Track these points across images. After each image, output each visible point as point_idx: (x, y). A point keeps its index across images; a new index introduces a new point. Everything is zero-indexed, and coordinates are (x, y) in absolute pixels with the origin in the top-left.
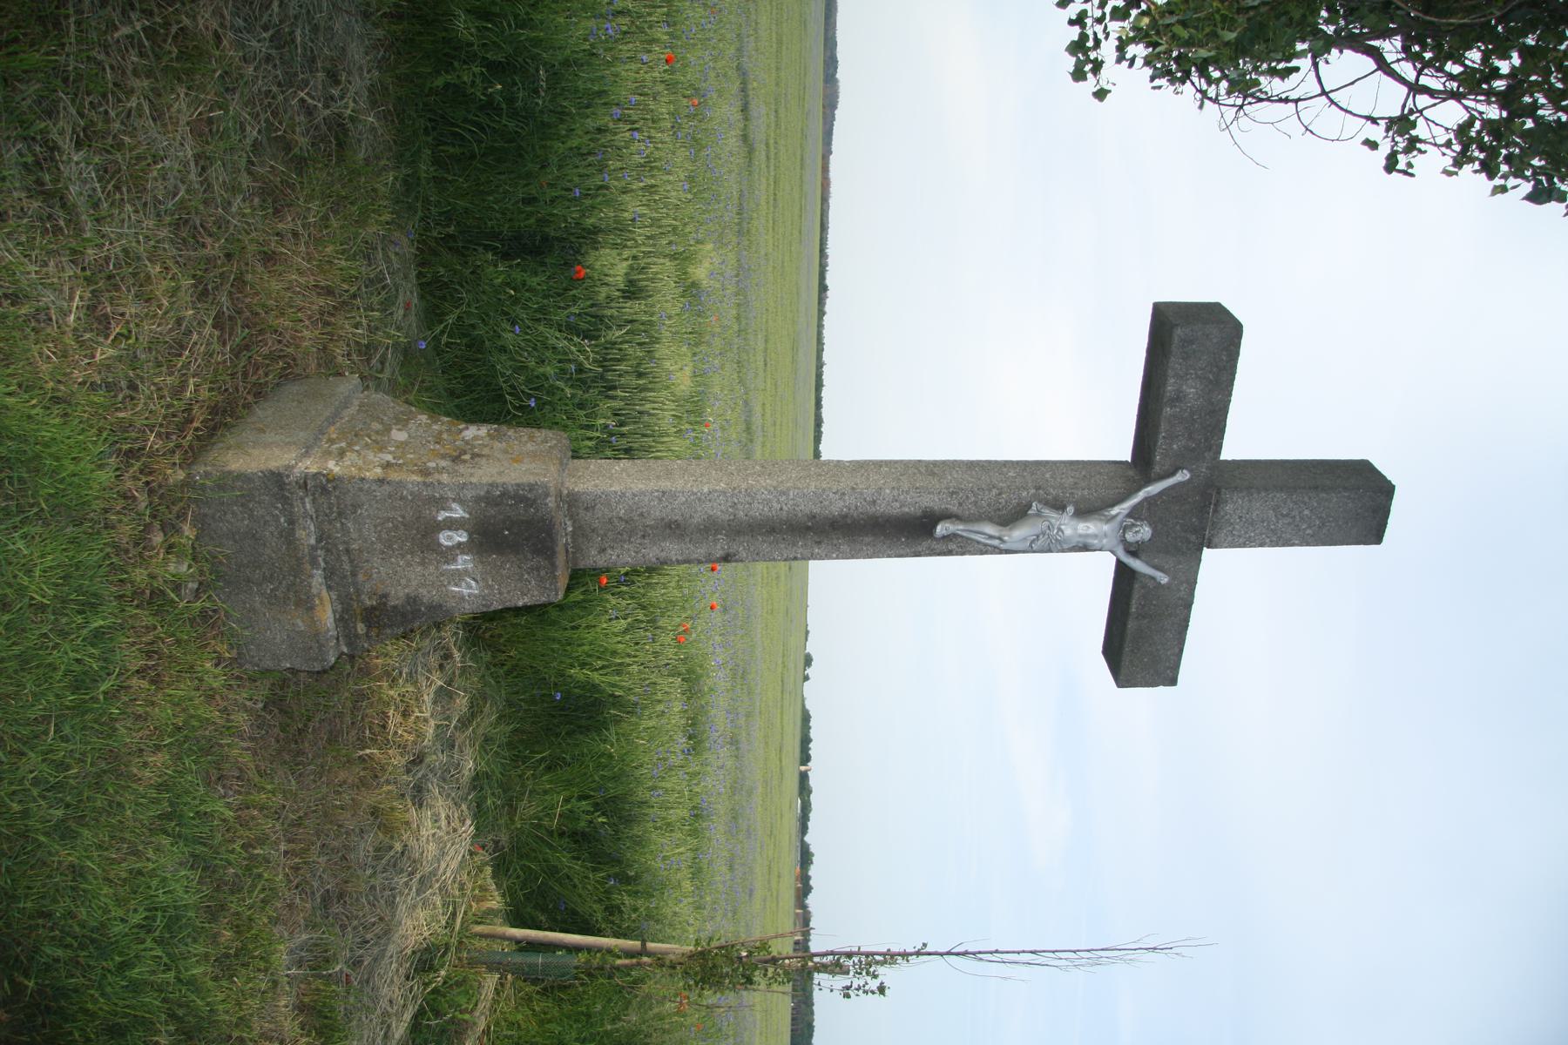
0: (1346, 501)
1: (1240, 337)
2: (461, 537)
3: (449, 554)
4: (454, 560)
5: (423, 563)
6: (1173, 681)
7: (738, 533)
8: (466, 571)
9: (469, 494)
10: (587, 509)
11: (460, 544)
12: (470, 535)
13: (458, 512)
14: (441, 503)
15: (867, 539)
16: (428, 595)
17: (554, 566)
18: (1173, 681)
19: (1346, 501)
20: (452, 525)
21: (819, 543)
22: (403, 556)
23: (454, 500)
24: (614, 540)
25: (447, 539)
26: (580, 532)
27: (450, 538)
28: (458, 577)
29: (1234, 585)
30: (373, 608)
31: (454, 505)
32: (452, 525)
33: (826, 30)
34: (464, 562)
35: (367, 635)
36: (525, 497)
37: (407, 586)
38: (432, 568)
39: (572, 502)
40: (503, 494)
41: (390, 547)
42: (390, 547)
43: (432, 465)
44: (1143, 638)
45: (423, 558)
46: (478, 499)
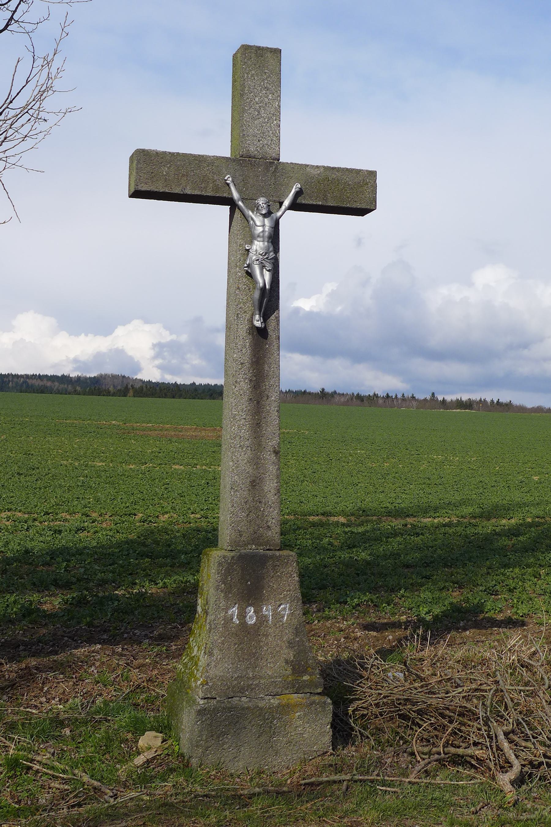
0: (256, 71)
1: (143, 150)
2: (251, 611)
3: (262, 620)
4: (266, 616)
5: (266, 636)
6: (373, 174)
7: (260, 445)
8: (275, 610)
9: (222, 604)
10: (241, 535)
11: (255, 612)
12: (250, 605)
13: (235, 610)
14: (228, 620)
15: (266, 367)
16: (288, 635)
17: (272, 557)
18: (373, 174)
19: (256, 71)
20: (242, 615)
21: (268, 397)
22: (261, 647)
23: (226, 613)
24: (262, 521)
25: (251, 618)
26: (256, 539)
27: (251, 617)
28: (277, 616)
29: (306, 140)
30: (294, 669)
31: (230, 612)
32: (242, 615)
33: (42, 390)
34: (267, 610)
35: (310, 675)
36: (227, 569)
37: (281, 647)
38: (270, 631)
39: (235, 544)
40: (224, 583)
41: (254, 654)
42: (254, 654)
43: (208, 627)
44: (345, 194)
45: (264, 635)
46: (226, 598)
